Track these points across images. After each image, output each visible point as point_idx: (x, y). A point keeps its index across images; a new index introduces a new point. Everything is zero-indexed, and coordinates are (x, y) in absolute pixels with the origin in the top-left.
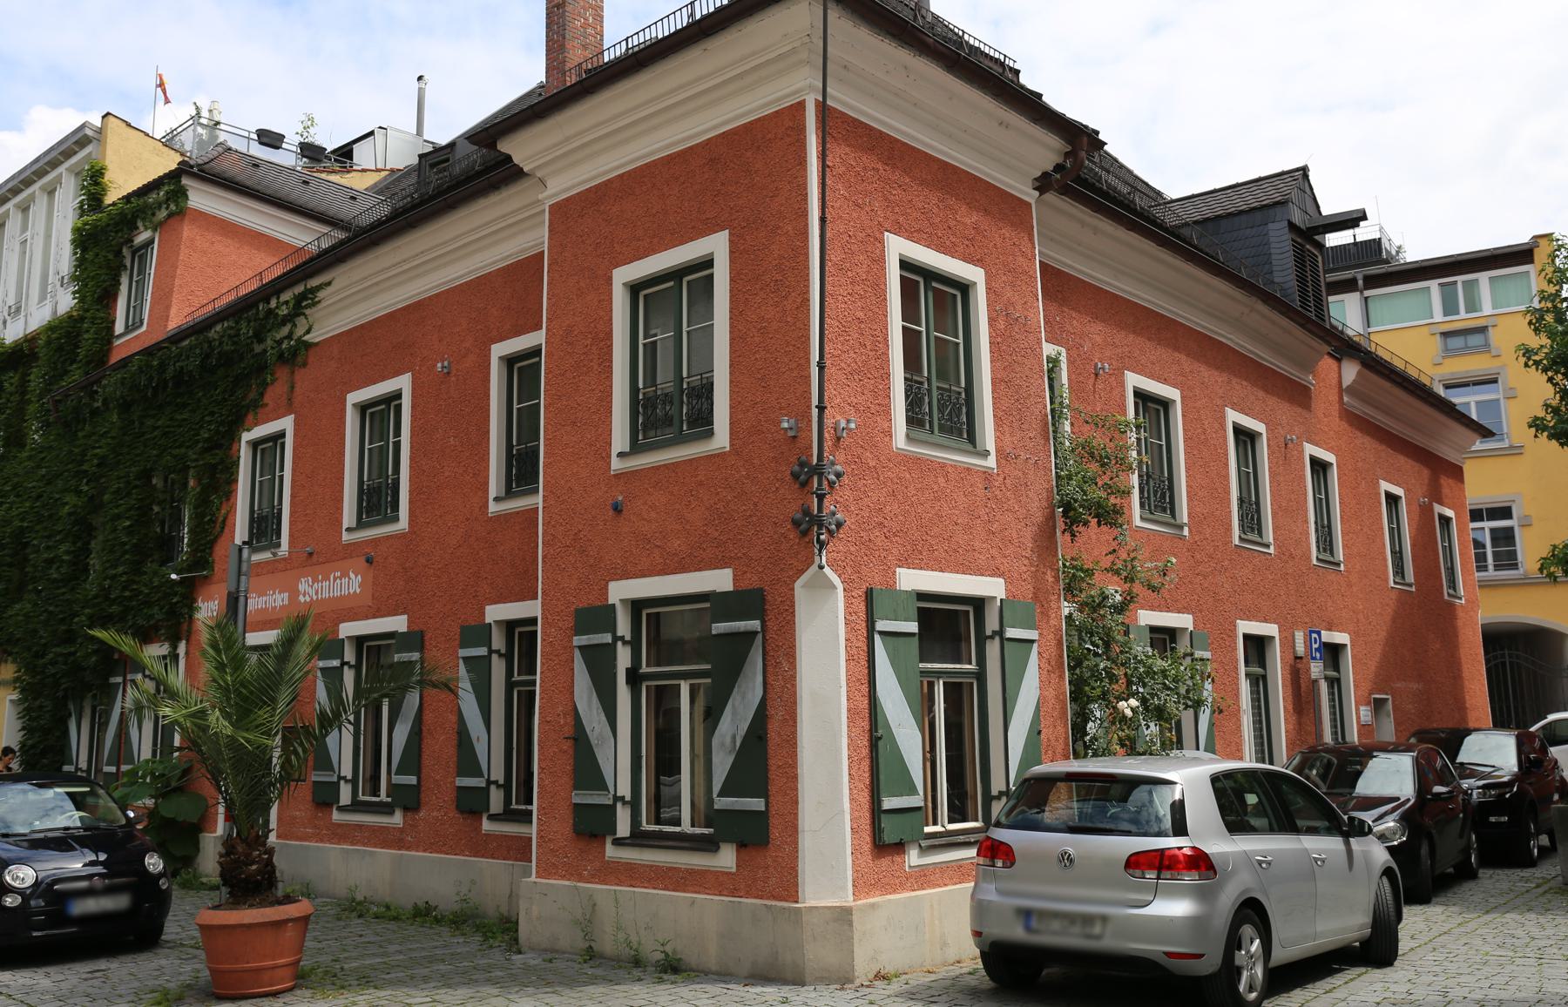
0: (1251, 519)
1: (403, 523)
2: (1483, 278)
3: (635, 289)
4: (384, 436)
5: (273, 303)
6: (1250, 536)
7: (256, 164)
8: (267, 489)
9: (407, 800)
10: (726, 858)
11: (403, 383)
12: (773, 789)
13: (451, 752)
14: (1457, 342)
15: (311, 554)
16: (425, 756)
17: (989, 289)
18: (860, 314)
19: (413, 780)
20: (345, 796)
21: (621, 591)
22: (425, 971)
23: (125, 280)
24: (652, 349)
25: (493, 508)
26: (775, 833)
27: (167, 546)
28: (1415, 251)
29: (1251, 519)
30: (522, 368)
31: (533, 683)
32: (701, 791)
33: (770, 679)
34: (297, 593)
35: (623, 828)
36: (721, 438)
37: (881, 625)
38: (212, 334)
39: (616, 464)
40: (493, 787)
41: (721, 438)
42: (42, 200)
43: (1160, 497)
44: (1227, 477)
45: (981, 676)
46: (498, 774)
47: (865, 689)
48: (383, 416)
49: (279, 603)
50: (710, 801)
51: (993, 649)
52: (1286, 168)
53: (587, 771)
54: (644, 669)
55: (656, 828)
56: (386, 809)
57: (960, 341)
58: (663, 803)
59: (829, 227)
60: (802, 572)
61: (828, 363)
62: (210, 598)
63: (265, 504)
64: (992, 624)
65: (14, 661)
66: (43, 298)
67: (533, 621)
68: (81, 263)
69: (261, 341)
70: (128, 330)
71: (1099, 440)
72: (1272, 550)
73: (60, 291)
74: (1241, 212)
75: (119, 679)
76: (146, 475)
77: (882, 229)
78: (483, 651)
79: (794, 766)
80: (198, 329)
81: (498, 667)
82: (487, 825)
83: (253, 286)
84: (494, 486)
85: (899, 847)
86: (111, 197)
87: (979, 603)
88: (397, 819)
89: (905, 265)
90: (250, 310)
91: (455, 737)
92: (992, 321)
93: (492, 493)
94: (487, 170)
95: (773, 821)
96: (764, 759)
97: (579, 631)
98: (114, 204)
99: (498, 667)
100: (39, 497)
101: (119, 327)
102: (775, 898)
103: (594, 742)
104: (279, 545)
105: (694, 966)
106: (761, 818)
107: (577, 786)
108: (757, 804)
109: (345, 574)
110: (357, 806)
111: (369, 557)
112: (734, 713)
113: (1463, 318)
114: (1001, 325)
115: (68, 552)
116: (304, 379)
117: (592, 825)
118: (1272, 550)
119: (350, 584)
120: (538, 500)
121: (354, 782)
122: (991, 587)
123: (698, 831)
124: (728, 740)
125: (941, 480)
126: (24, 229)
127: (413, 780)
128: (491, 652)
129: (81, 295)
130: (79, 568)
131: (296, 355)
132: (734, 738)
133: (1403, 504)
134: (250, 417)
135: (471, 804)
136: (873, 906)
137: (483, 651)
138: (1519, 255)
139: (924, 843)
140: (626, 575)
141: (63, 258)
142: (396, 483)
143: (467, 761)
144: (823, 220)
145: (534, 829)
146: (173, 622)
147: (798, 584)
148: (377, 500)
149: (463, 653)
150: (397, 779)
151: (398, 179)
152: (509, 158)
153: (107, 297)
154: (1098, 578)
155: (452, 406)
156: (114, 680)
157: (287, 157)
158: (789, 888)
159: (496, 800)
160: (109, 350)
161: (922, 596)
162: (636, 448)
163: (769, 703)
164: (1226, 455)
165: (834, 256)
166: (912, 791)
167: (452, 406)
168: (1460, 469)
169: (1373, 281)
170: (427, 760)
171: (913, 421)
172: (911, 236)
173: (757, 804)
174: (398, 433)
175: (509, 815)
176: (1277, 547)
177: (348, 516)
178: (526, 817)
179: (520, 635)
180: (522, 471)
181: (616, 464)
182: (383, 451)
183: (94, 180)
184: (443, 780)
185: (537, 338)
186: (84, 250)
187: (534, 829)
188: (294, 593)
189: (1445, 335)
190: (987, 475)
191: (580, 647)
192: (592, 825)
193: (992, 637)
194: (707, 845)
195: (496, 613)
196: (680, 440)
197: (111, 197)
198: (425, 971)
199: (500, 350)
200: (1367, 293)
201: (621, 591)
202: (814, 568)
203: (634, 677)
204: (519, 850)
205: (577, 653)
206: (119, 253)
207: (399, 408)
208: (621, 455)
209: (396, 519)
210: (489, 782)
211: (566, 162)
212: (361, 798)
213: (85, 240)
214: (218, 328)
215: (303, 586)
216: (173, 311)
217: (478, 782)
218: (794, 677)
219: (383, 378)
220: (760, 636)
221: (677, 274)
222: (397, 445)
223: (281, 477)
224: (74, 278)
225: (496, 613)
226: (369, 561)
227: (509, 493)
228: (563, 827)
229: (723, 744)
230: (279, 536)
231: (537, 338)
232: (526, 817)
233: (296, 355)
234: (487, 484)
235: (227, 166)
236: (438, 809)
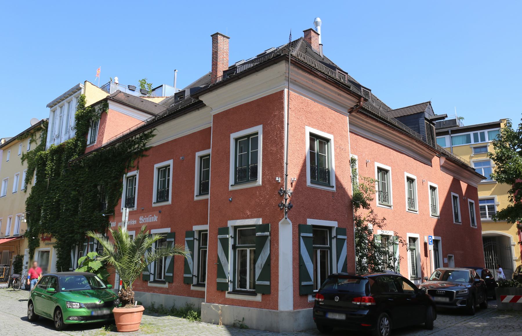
0: (412, 202)
1: (170, 202)
2: (486, 131)
3: (236, 140)
4: (165, 177)
5: (134, 138)
6: (411, 209)
7: (128, 96)
8: (131, 191)
9: (170, 280)
10: (259, 298)
11: (170, 162)
12: (272, 279)
13: (182, 266)
14: (478, 150)
15: (143, 210)
16: (175, 268)
17: (335, 141)
18: (298, 149)
19: (171, 275)
20: (152, 278)
21: (231, 224)
22: (176, 328)
23: (90, 129)
24: (241, 156)
25: (196, 199)
26: (272, 291)
27: (101, 206)
28: (465, 123)
29: (412, 202)
30: (205, 161)
31: (206, 248)
32: (252, 281)
33: (272, 248)
34: (139, 220)
35: (230, 289)
36: (260, 181)
37: (302, 234)
38: (116, 146)
39: (231, 188)
40: (194, 277)
41: (260, 181)
42: (66, 105)
43: (384, 197)
44: (404, 192)
45: (330, 248)
46: (195, 273)
47: (298, 252)
48: (165, 171)
49: (134, 223)
50: (254, 282)
51: (334, 241)
52: (425, 102)
53: (221, 273)
54: (237, 245)
55: (239, 289)
56: (164, 282)
57: (326, 155)
58: (243, 284)
59: (289, 125)
60: (280, 220)
61: (288, 162)
62: (113, 221)
63: (130, 195)
64: (334, 234)
65: (56, 238)
66: (66, 133)
67: (207, 231)
68: (77, 124)
69: (130, 148)
70: (91, 143)
71: (366, 184)
72: (417, 213)
73: (71, 131)
74: (411, 115)
75: (87, 244)
76: (95, 186)
77: (305, 125)
78: (192, 239)
79: (278, 273)
80: (112, 144)
81: (196, 243)
82: (192, 288)
83: (128, 131)
84: (196, 192)
85: (306, 295)
86: (86, 106)
87: (330, 228)
88: (166, 285)
89: (311, 135)
90: (126, 140)
91: (183, 263)
92: (335, 150)
93: (196, 194)
94: (195, 103)
95: (272, 288)
96: (269, 270)
97: (220, 233)
98: (88, 107)
99: (196, 243)
100: (64, 191)
101: (88, 143)
102: (272, 309)
103: (223, 265)
104: (134, 207)
105: (249, 326)
106: (269, 287)
107: (185, 273)
108: (267, 283)
109: (153, 216)
110: (155, 281)
111: (160, 211)
112: (262, 258)
113: (480, 143)
114: (338, 150)
115: (72, 207)
116: (143, 162)
117: (222, 288)
118: (417, 213)
119: (154, 219)
120: (208, 197)
121: (154, 275)
122: (334, 224)
123: (251, 290)
124: (260, 265)
125: (320, 194)
126: (61, 113)
127: (171, 275)
128: (194, 239)
129: (77, 134)
130: (76, 211)
131: (142, 153)
132: (261, 265)
133: (458, 199)
134: (126, 170)
135: (188, 282)
136: (299, 312)
137: (192, 239)
138: (497, 125)
139: (314, 295)
140: (233, 219)
141: (73, 122)
142: (168, 190)
143: (187, 270)
144: (288, 124)
145: (205, 289)
146: (102, 227)
147: (280, 223)
148: (162, 196)
149: (186, 239)
150: (166, 274)
151: (168, 100)
152: (202, 101)
153: (85, 134)
154: (365, 223)
155: (184, 169)
156: (84, 244)
157: (137, 94)
158: (276, 307)
159: (195, 280)
160: (85, 149)
161: (314, 226)
162: (236, 183)
163: (272, 257)
164: (404, 185)
165: (291, 133)
166: (310, 280)
167: (184, 169)
168: (477, 189)
169: (453, 132)
170: (175, 269)
171: (313, 176)
172: (313, 126)
173: (267, 283)
174: (169, 176)
175: (198, 285)
176: (420, 212)
177: (154, 199)
178: (204, 285)
179: (203, 235)
180: (204, 189)
181: (231, 188)
182: (164, 181)
183: (82, 101)
184: (180, 275)
185: (209, 151)
186: (79, 121)
187: (205, 289)
188: (138, 220)
189: (474, 148)
190: (333, 193)
191: (220, 239)
192: (222, 288)
193: (334, 238)
194: (254, 294)
195: (196, 228)
196: (248, 181)
197: (86, 106)
198: (176, 328)
199: (198, 154)
200: (452, 135)
201: (231, 224)
202: (284, 219)
203: (234, 247)
204: (201, 295)
205: (219, 240)
206: (89, 122)
207: (169, 169)
208: (232, 185)
209: (168, 200)
210: (193, 276)
211: (217, 102)
212: (156, 279)
213: (78, 118)
214: (118, 144)
215: (141, 219)
216: (104, 139)
217: (190, 276)
218: (278, 248)
219: (165, 161)
220: (270, 237)
221: (248, 136)
222: (169, 180)
223: (135, 188)
224: (75, 128)
225: (196, 228)
226: (160, 212)
227: (200, 194)
228: (214, 288)
229: (258, 266)
230: (134, 204)
231: (209, 151)
232: (204, 285)
233: (142, 153)
234: (194, 191)
235: (121, 97)
236: (178, 283)
